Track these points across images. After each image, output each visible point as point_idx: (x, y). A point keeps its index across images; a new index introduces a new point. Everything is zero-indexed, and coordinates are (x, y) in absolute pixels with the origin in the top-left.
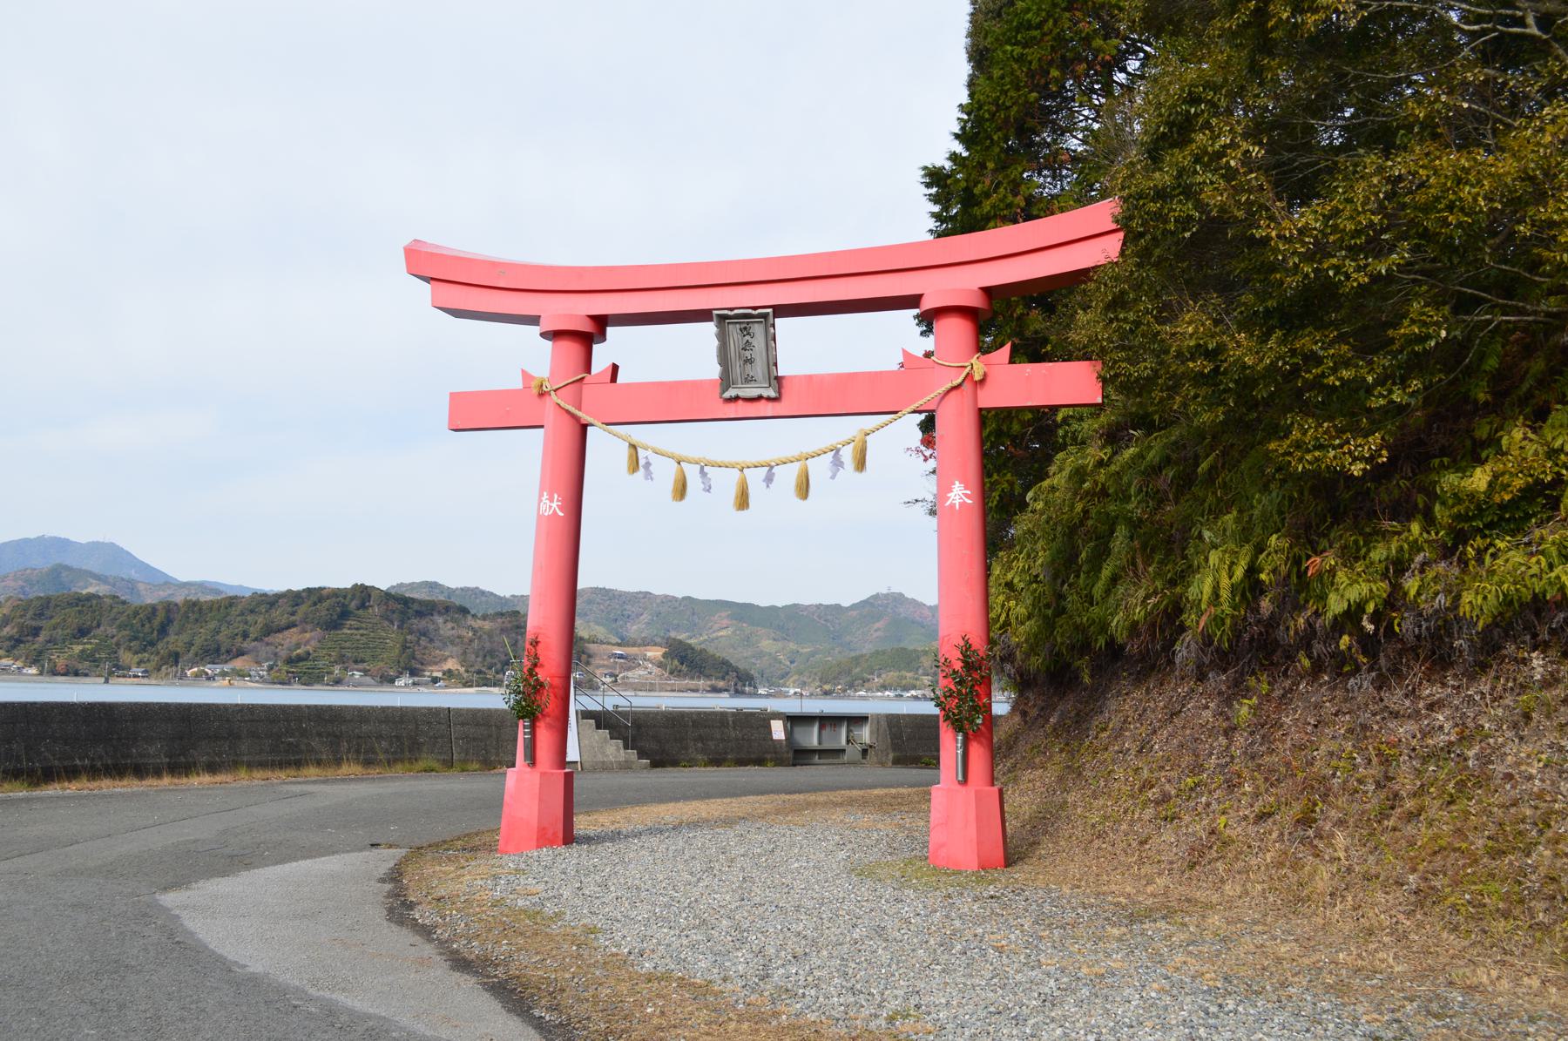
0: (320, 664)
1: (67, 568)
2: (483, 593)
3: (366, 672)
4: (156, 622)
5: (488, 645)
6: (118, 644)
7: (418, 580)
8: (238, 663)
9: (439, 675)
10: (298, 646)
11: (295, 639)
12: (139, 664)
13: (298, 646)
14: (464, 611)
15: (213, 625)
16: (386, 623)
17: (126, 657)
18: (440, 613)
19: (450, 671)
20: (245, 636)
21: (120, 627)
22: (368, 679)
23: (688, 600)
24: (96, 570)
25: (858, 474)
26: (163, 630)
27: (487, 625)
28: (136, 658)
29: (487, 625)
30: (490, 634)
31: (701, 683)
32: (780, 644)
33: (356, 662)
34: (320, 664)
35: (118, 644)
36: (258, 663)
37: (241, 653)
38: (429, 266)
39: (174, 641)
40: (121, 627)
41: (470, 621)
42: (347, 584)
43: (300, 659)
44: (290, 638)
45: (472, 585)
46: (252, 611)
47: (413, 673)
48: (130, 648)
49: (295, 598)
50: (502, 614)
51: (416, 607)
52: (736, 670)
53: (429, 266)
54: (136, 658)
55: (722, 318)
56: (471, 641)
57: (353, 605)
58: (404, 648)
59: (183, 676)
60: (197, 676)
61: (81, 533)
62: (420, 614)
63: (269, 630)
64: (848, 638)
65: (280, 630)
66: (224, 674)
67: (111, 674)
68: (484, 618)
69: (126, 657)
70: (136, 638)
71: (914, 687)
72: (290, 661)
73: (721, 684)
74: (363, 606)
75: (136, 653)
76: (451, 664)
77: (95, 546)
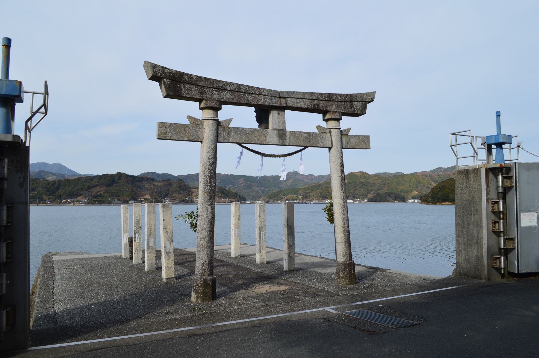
0: (105, 197)
1: (43, 171)
2: (169, 175)
3: (119, 200)
4: (55, 186)
5: (159, 190)
6: (43, 193)
7: (149, 172)
8: (79, 198)
9: (143, 200)
10: (99, 192)
11: (98, 190)
12: (49, 199)
13: (99, 192)
14: (153, 180)
15: (73, 186)
16: (127, 184)
17: (45, 197)
18: (145, 181)
19: (146, 198)
20: (82, 189)
21: (44, 188)
22: (120, 202)
23: (232, 175)
24: (52, 172)
25: (372, 142)
26: (58, 188)
27: (160, 184)
28: (48, 198)
29: (160, 184)
30: (160, 187)
31: (227, 200)
32: (259, 188)
33: (117, 196)
34: (105, 197)
35: (43, 193)
36: (86, 198)
37: (80, 195)
38: (158, 74)
39: (61, 192)
40: (44, 188)
41: (154, 183)
42: (115, 172)
43: (98, 196)
44: (97, 189)
45: (165, 172)
46: (86, 182)
47: (134, 199)
48: (46, 194)
49: (99, 177)
50: (165, 180)
51: (137, 179)
52: (239, 196)
53: (158, 74)
54: (48, 198)
55: (34, 93)
56: (154, 189)
57: (116, 179)
58: (132, 191)
59: (61, 202)
60: (65, 202)
61: (50, 161)
62: (139, 181)
63: (89, 188)
64: (281, 185)
65: (93, 187)
66: (73, 202)
67: (39, 203)
68: (159, 182)
69: (45, 197)
70: (49, 191)
71: (297, 200)
72: (94, 197)
73: (234, 200)
74: (119, 179)
75: (48, 196)
76: (147, 196)
77: (55, 165)
